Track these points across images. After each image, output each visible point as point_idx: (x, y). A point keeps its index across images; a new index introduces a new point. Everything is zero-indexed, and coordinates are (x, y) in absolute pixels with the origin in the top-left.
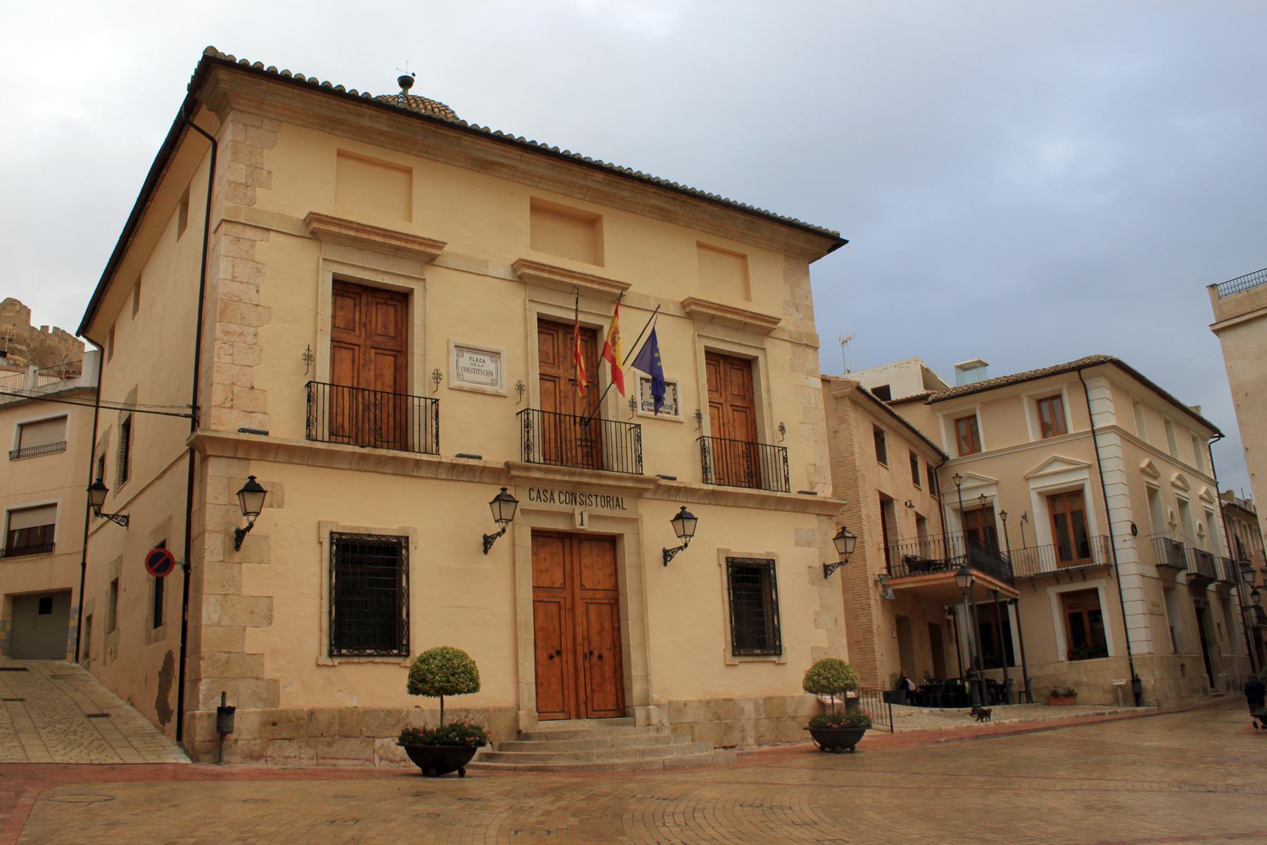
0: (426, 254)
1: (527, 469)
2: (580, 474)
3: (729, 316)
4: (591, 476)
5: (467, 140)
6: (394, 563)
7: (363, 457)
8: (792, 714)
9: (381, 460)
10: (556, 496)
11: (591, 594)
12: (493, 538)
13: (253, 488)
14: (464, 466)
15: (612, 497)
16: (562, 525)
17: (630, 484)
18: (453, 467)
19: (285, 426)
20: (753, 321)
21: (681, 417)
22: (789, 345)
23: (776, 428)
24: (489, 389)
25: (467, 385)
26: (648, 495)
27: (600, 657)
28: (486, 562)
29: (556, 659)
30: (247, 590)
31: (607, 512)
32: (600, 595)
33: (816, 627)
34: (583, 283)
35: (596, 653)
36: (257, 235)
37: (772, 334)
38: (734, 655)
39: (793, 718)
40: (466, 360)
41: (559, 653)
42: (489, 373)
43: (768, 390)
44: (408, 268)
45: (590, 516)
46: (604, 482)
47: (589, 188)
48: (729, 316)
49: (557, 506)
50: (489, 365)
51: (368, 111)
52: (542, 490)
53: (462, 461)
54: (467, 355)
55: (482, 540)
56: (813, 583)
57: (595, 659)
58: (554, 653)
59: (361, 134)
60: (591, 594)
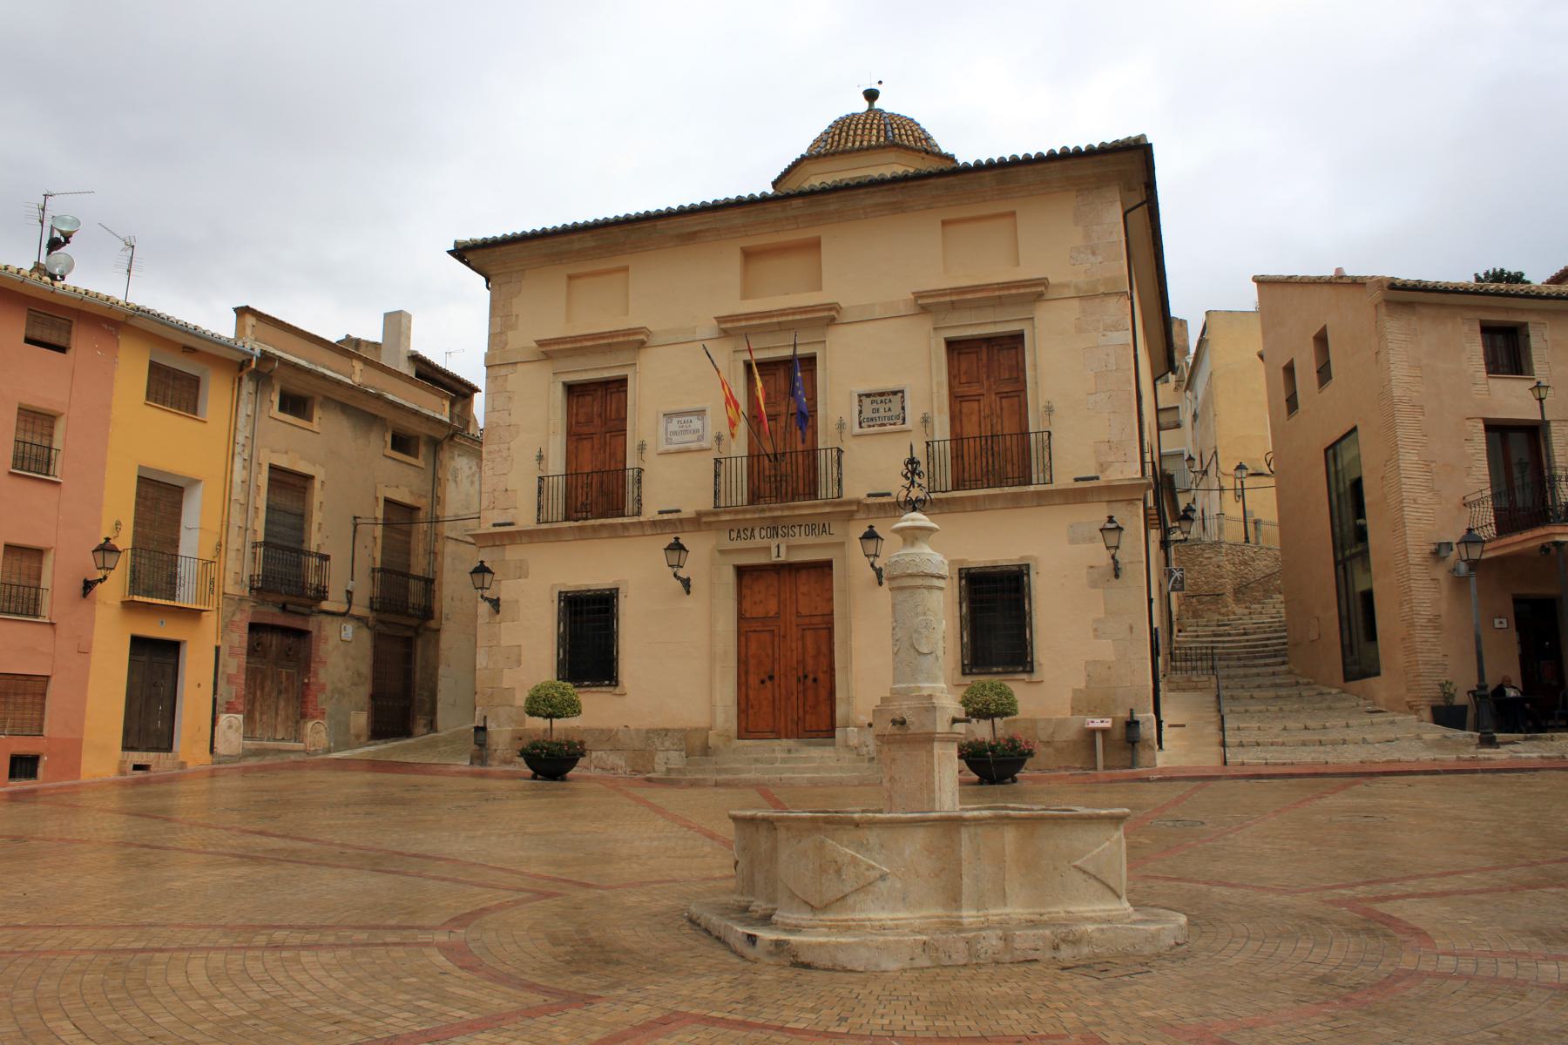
0: (635, 342)
1: (716, 514)
2: (771, 510)
3: (969, 296)
4: (782, 509)
5: (660, 224)
6: (607, 611)
7: (580, 528)
8: (1045, 738)
9: (594, 528)
10: (756, 533)
11: (807, 620)
12: (94, 583)
13: (482, 569)
14: (663, 521)
15: (817, 526)
16: (761, 559)
17: (827, 510)
18: (654, 523)
19: (526, 519)
20: (1006, 292)
21: (908, 425)
22: (1076, 303)
23: (1041, 409)
24: (693, 446)
25: (673, 447)
26: (858, 516)
27: (815, 680)
28: (688, 602)
29: (768, 683)
30: (503, 643)
31: (811, 540)
32: (815, 620)
33: (1096, 637)
34: (784, 319)
35: (811, 677)
36: (510, 369)
37: (1047, 296)
38: (964, 673)
39: (1048, 744)
40: (674, 425)
41: (771, 678)
42: (695, 431)
43: (1035, 366)
44: (624, 357)
45: (788, 548)
46: (797, 512)
47: (795, 217)
48: (969, 296)
49: (758, 542)
50: (696, 423)
51: (574, 237)
52: (740, 530)
53: (666, 517)
54: (675, 420)
55: (81, 585)
56: (1094, 584)
57: (809, 682)
58: (765, 677)
59: (581, 255)
60: (807, 620)
